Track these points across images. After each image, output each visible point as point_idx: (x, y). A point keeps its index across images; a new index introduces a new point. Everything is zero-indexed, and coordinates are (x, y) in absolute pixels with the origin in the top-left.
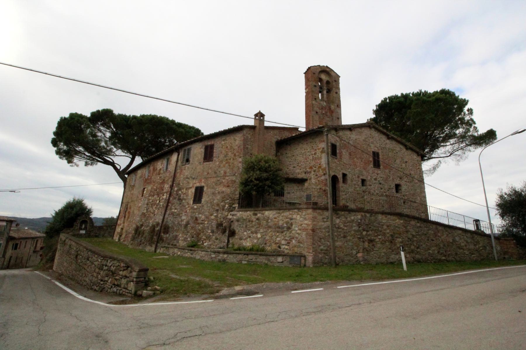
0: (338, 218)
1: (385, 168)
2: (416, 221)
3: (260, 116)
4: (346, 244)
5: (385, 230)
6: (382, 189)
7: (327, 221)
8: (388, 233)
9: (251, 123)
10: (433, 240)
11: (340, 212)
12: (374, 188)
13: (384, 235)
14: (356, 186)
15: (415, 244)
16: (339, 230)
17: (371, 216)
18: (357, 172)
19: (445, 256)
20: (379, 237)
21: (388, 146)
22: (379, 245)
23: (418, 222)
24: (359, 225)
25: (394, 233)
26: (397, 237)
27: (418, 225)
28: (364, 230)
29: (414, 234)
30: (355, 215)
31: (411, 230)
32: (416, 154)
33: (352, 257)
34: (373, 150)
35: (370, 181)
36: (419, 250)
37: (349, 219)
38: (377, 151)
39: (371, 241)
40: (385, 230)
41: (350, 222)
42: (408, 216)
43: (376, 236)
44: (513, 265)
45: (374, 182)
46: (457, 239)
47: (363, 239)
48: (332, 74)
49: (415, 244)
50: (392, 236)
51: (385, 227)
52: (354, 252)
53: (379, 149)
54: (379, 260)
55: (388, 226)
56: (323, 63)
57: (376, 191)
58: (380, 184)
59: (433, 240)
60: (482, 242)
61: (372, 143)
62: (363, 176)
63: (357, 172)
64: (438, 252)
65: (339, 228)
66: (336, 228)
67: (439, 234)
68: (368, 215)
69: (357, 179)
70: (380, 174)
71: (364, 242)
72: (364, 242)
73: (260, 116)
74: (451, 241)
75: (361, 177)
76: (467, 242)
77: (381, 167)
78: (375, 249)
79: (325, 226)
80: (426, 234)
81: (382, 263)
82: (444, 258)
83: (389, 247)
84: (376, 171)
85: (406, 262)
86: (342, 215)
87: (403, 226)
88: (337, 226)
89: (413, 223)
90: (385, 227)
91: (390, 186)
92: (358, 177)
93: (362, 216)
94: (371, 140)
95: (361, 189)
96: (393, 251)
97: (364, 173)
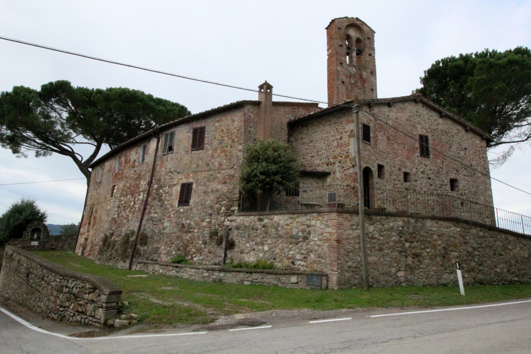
0: (372, 224)
2: (479, 229)
3: (266, 88)
4: (382, 260)
5: (436, 240)
6: (431, 185)
7: (357, 229)
9: (255, 97)
10: (501, 255)
11: (374, 217)
13: (434, 247)
14: (397, 182)
15: (476, 260)
16: (373, 241)
17: (416, 222)
19: (518, 276)
22: (426, 261)
23: (481, 231)
24: (400, 234)
27: (481, 234)
28: (407, 241)
29: (475, 245)
30: (395, 221)
31: (472, 241)
32: (480, 138)
33: (391, 277)
35: (414, 174)
36: (481, 268)
37: (386, 226)
38: (426, 134)
42: (467, 222)
43: (423, 249)
45: (421, 175)
47: (405, 252)
48: (364, 28)
49: (476, 260)
50: (444, 248)
51: (435, 237)
52: (393, 270)
53: (427, 132)
54: (426, 280)
55: (439, 236)
57: (424, 189)
58: (429, 178)
59: (501, 255)
64: (509, 271)
66: (369, 238)
67: (510, 247)
68: (412, 221)
71: (406, 257)
72: (406, 257)
74: (527, 256)
75: (404, 170)
80: (491, 247)
81: (431, 285)
82: (516, 279)
83: (441, 263)
86: (377, 221)
87: (460, 235)
88: (370, 236)
89: (474, 231)
90: (435, 237)
91: (443, 181)
92: (400, 169)
93: (404, 222)
96: (445, 269)
97: (408, 163)
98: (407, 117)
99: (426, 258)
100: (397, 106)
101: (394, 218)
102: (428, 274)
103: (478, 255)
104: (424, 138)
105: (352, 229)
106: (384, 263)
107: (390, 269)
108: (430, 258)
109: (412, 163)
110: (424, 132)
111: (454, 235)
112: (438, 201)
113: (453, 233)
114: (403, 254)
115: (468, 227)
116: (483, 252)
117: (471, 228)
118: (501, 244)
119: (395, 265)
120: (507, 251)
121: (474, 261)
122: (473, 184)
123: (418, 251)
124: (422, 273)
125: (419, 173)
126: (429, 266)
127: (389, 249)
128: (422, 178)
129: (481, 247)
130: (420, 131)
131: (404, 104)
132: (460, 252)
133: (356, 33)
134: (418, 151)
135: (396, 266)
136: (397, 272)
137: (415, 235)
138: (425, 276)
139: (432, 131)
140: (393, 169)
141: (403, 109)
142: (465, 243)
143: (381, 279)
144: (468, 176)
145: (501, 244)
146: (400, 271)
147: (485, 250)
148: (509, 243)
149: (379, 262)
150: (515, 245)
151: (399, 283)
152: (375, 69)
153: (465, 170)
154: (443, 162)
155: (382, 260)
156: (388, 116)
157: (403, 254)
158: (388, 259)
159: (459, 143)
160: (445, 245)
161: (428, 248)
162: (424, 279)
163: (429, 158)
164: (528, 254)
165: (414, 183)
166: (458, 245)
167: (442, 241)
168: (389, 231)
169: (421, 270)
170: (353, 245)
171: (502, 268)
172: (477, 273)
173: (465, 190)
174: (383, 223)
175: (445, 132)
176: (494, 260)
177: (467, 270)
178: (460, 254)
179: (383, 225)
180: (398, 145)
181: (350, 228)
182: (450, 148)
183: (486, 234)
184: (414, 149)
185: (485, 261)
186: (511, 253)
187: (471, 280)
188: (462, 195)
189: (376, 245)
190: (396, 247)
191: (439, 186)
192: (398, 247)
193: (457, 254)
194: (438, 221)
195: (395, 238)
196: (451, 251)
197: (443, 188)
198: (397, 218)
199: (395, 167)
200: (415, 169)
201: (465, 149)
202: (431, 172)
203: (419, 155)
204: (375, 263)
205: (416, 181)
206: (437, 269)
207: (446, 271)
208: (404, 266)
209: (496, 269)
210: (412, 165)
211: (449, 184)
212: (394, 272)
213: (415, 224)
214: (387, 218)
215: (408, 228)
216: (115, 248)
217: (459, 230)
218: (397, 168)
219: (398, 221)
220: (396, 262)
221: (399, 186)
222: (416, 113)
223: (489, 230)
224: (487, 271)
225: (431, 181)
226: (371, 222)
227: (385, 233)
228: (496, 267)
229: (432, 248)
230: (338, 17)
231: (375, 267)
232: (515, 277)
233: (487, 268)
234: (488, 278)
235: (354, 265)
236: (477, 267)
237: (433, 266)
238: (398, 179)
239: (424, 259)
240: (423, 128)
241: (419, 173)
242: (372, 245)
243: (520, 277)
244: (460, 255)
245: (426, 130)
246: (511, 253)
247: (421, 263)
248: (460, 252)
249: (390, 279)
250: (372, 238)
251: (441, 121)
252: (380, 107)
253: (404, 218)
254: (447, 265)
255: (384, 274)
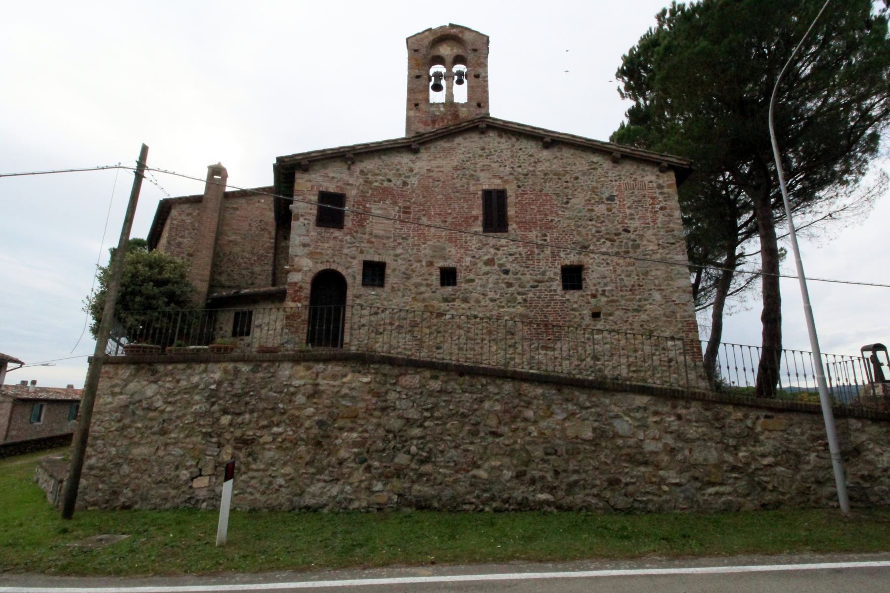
0: (155, 382)
1: (525, 226)
2: (427, 374)
3: (217, 173)
4: (161, 453)
5: (300, 408)
6: (509, 285)
7: (121, 393)
8: (309, 417)
9: (199, 189)
10: (495, 434)
11: (161, 368)
12: (482, 288)
13: (295, 421)
14: (423, 289)
15: (413, 449)
16: (151, 414)
17: (254, 371)
18: (428, 251)
19: (552, 490)
21: (541, 167)
22: (269, 454)
23: (435, 378)
24: (212, 397)
25: (330, 415)
26: (341, 429)
27: (435, 385)
28: (225, 412)
29: (413, 414)
30: (205, 371)
31: (402, 404)
32: (656, 170)
33: (177, 488)
34: (486, 187)
35: (468, 269)
36: (427, 468)
37: (183, 383)
39: (244, 442)
41: (186, 391)
42: (391, 361)
43: (264, 427)
44: (823, 547)
45: (485, 269)
47: (219, 436)
48: (467, 37)
49: (413, 449)
51: (300, 399)
52: (185, 474)
53: (506, 182)
54: (263, 498)
56: (438, 21)
57: (491, 295)
58: (506, 272)
59: (495, 434)
63: (428, 251)
64: (519, 476)
65: (149, 409)
66: (144, 409)
67: (530, 414)
68: (245, 368)
70: (504, 247)
71: (220, 445)
72: (220, 445)
73: (217, 173)
74: (588, 434)
75: (441, 264)
78: (254, 466)
80: (464, 415)
81: (272, 510)
84: (492, 240)
86: (166, 375)
87: (371, 391)
89: (412, 380)
90: (300, 399)
91: (544, 274)
92: (430, 264)
93: (226, 371)
96: (320, 471)
97: (452, 250)
98: (455, 164)
99: (267, 446)
100: (433, 149)
101: (203, 366)
102: (270, 483)
104: (494, 196)
105: (113, 394)
107: (177, 473)
109: (462, 247)
110: (496, 184)
111: (354, 393)
112: (527, 317)
113: (352, 389)
114: (214, 440)
118: (498, 407)
119: (188, 464)
120: (521, 425)
121: (408, 452)
123: (251, 433)
124: (253, 482)
126: (273, 465)
127: (183, 429)
130: (488, 183)
131: (453, 141)
132: (366, 431)
133: (452, 50)
134: (480, 222)
135: (191, 466)
136: (192, 479)
137: (248, 399)
138: (263, 488)
139: (518, 179)
140: (415, 265)
141: (447, 152)
142: (384, 409)
143: (153, 492)
145: (498, 407)
146: (200, 475)
147: (445, 424)
148: (528, 404)
149: (154, 457)
151: (193, 502)
152: (487, 98)
153: (608, 243)
154: (545, 235)
156: (411, 170)
157: (214, 440)
158: (177, 451)
159: (594, 190)
160: (324, 417)
164: (594, 430)
165: (464, 286)
166: (361, 415)
168: (185, 393)
169: (251, 474)
171: (499, 468)
172: (413, 482)
173: (606, 285)
176: (471, 448)
177: (381, 474)
178: (367, 435)
179: (178, 381)
180: (429, 219)
182: (567, 203)
185: (442, 452)
186: (532, 428)
187: (390, 499)
189: (155, 423)
190: (199, 425)
191: (532, 283)
192: (203, 426)
194: (311, 364)
196: (341, 429)
198: (210, 366)
199: (420, 261)
200: (468, 259)
201: (611, 198)
204: (144, 460)
205: (472, 281)
206: (296, 470)
207: (322, 477)
208: (211, 465)
209: (475, 472)
210: (462, 251)
211: (558, 278)
212: (184, 478)
214: (189, 368)
215: (232, 384)
217: (365, 380)
218: (424, 263)
219: (213, 372)
220: (192, 457)
221: (426, 295)
222: (480, 152)
223: (461, 374)
224: (445, 476)
225: (510, 278)
226: (152, 378)
227: (179, 397)
228: (479, 467)
232: (542, 491)
233: (446, 467)
235: (100, 465)
237: (285, 464)
238: (425, 282)
240: (495, 176)
243: (560, 494)
244: (365, 438)
245: (501, 178)
246: (532, 428)
248: (366, 431)
249: (173, 492)
250: (149, 409)
251: (545, 154)
252: (384, 157)
253: (224, 365)
255: (160, 482)
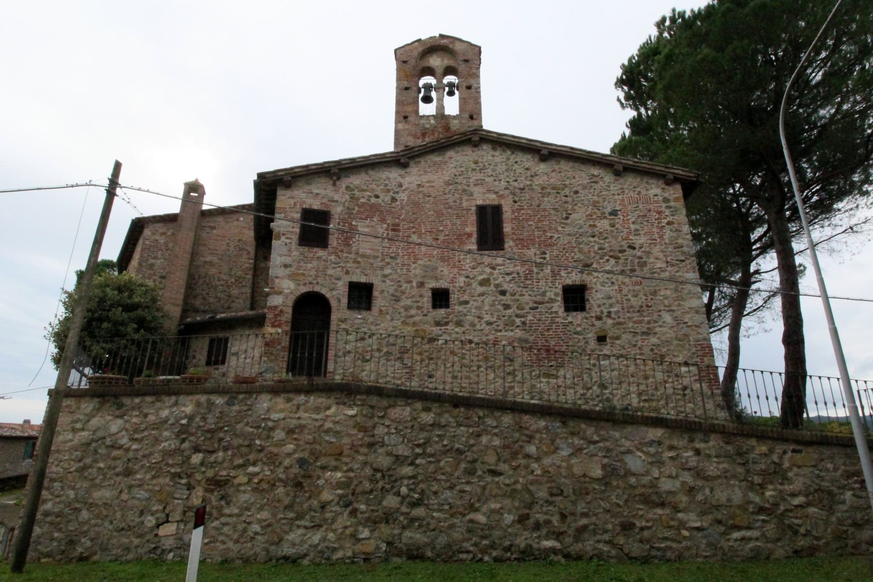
0: (121, 417)
1: (522, 243)
2: (419, 405)
3: (194, 189)
4: (124, 496)
5: (281, 444)
6: (507, 307)
7: (83, 430)
8: (289, 455)
9: (174, 207)
10: (494, 473)
11: (127, 401)
12: (477, 310)
13: (273, 460)
14: (413, 312)
15: (404, 490)
16: (116, 453)
17: (229, 403)
19: (558, 535)
20: (251, 469)
21: (538, 181)
22: (244, 497)
23: (427, 410)
24: (183, 433)
26: (324, 468)
28: (196, 449)
29: (403, 450)
30: (176, 404)
32: (661, 183)
34: (480, 202)
35: (462, 290)
36: (419, 512)
37: (151, 418)
38: (496, 203)
39: (216, 484)
40: (281, 444)
42: (377, 391)
43: (240, 466)
45: (480, 289)
46: (635, 462)
47: (189, 476)
48: (458, 47)
49: (404, 490)
50: (302, 462)
52: (150, 521)
55: (290, 431)
56: (428, 31)
57: (487, 318)
58: (503, 293)
59: (494, 473)
60: (801, 473)
61: (479, 183)
62: (437, 279)
63: (417, 271)
64: (522, 520)
67: (532, 449)
69: (415, 291)
70: (500, 266)
71: (190, 487)
73: (194, 189)
74: (598, 473)
75: (433, 284)
76: (699, 474)
77: (509, 244)
78: (227, 511)
79: (76, 442)
80: (459, 452)
82: (548, 544)
83: (287, 501)
85: (202, 562)
86: (133, 409)
87: (357, 425)
88: (108, 441)
89: (402, 412)
90: (279, 434)
91: (544, 294)
92: (421, 285)
93: (198, 404)
94: (475, 177)
95: (429, 318)
96: (300, 516)
97: (445, 270)
98: (447, 178)
99: (243, 488)
100: (423, 163)
102: (245, 530)
103: (410, 478)
105: (74, 430)
106: (130, 503)
108: (255, 490)
109: (454, 266)
111: (338, 428)
115: (385, 403)
116: (431, 468)
117: (394, 406)
118: (497, 442)
119: (155, 508)
121: (398, 494)
122: (637, 288)
124: (226, 529)
125: (475, 285)
126: (248, 509)
128: (483, 294)
129: (424, 454)
130: (482, 197)
131: (444, 154)
132: (351, 470)
133: (443, 60)
136: (158, 526)
137: (221, 435)
139: (514, 194)
140: (405, 286)
142: (371, 445)
143: (115, 541)
144: (622, 272)
145: (497, 442)
146: (167, 521)
148: (530, 439)
149: (117, 502)
150: (553, 441)
151: (159, 552)
155: (124, 496)
156: (400, 185)
157: (184, 481)
160: (305, 455)
161: (254, 464)
162: (230, 544)
163: (502, 248)
167: (297, 445)
168: (153, 429)
169: (224, 520)
170: (66, 466)
171: (498, 512)
173: (611, 306)
174: (145, 411)
175: (553, 188)
176: (468, 488)
177: (368, 519)
178: (352, 475)
179: (146, 416)
181: (69, 428)
183: (446, 418)
184: (462, 237)
186: (535, 465)
187: (378, 548)
188: (599, 318)
190: (167, 464)
191: (531, 305)
192: (172, 466)
193: (339, 475)
194: (291, 395)
195: (166, 444)
197: (542, 308)
200: (462, 279)
201: (614, 213)
202: (508, 278)
203: (474, 247)
205: (467, 302)
206: (274, 515)
207: (303, 523)
208: (180, 510)
210: (456, 270)
211: (559, 298)
212: (150, 525)
213: (226, 409)
215: (204, 419)
216: (81, 464)
217: (351, 412)
218: (414, 284)
221: (417, 319)
223: (456, 406)
225: (507, 299)
226: (117, 413)
229: (264, 463)
230: (402, 45)
231: (105, 512)
232: (547, 537)
234: (442, 540)
235: (56, 510)
236: (404, 509)
237: (261, 508)
238: (416, 305)
239: (238, 491)
241: (475, 285)
242: (110, 462)
243: (568, 540)
244: (350, 478)
245: (496, 193)
247: (228, 503)
248: (351, 470)
249: (136, 541)
251: (543, 167)
253: (197, 397)
254: (305, 506)
255: (123, 529)
